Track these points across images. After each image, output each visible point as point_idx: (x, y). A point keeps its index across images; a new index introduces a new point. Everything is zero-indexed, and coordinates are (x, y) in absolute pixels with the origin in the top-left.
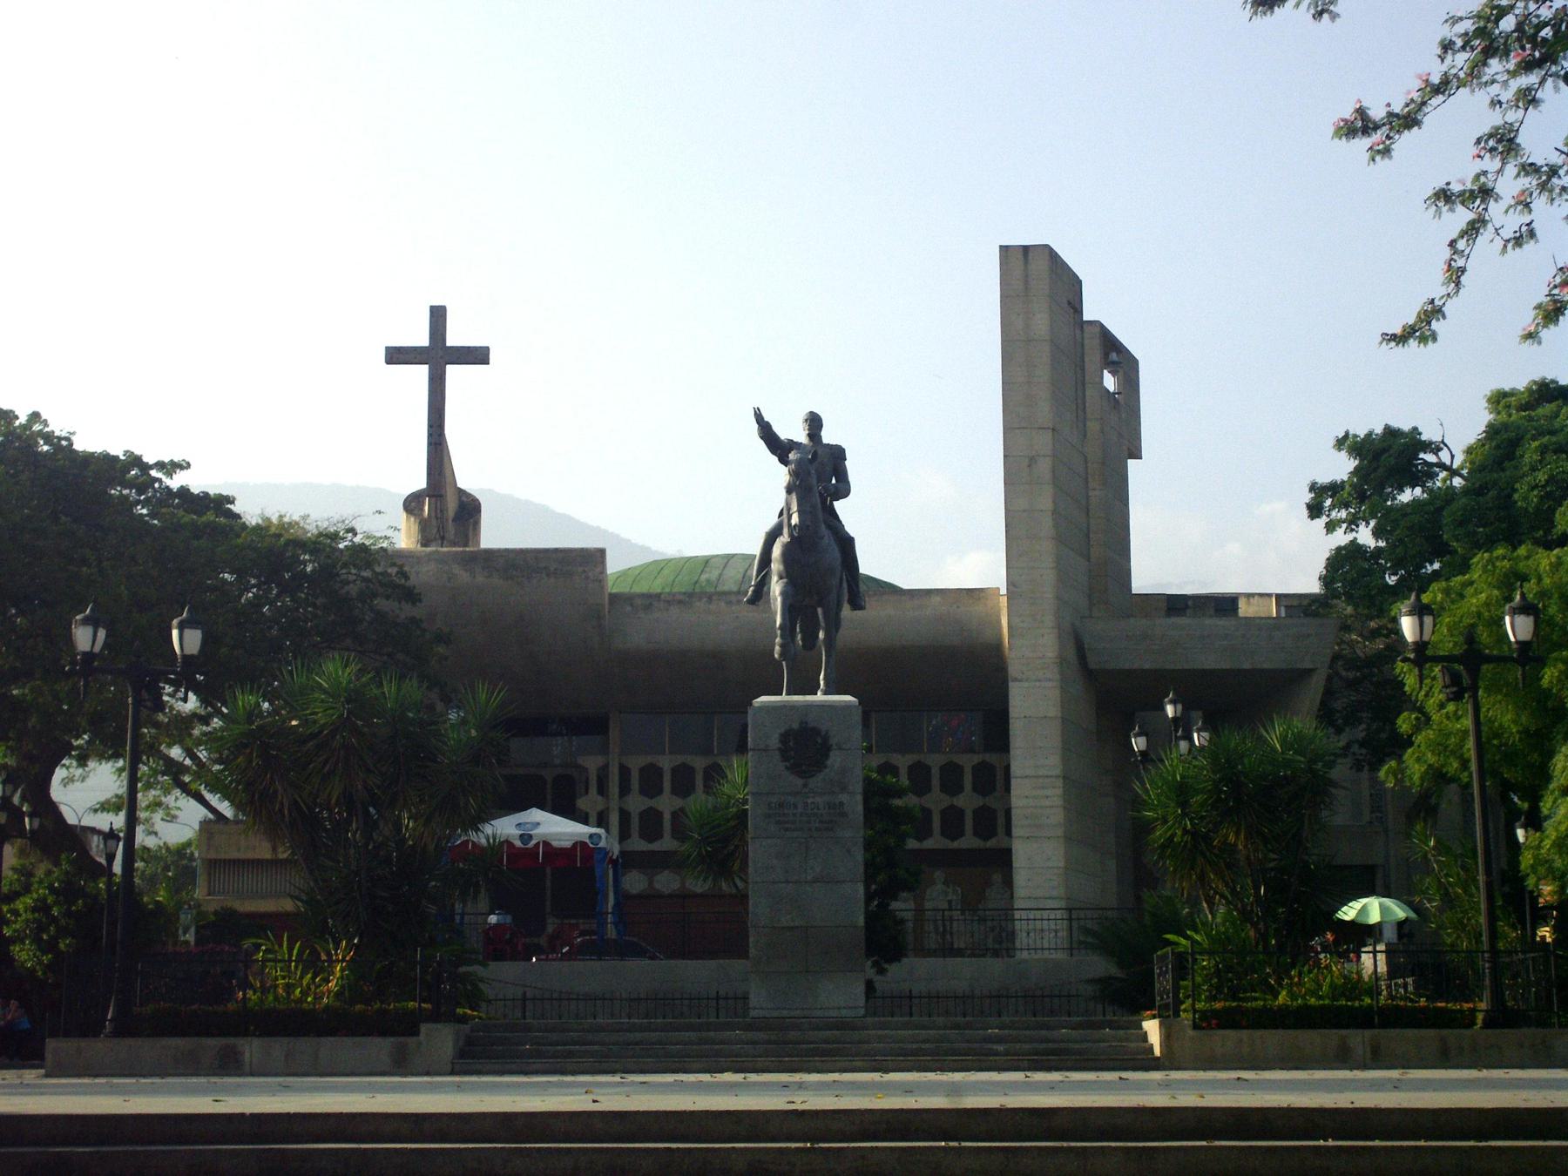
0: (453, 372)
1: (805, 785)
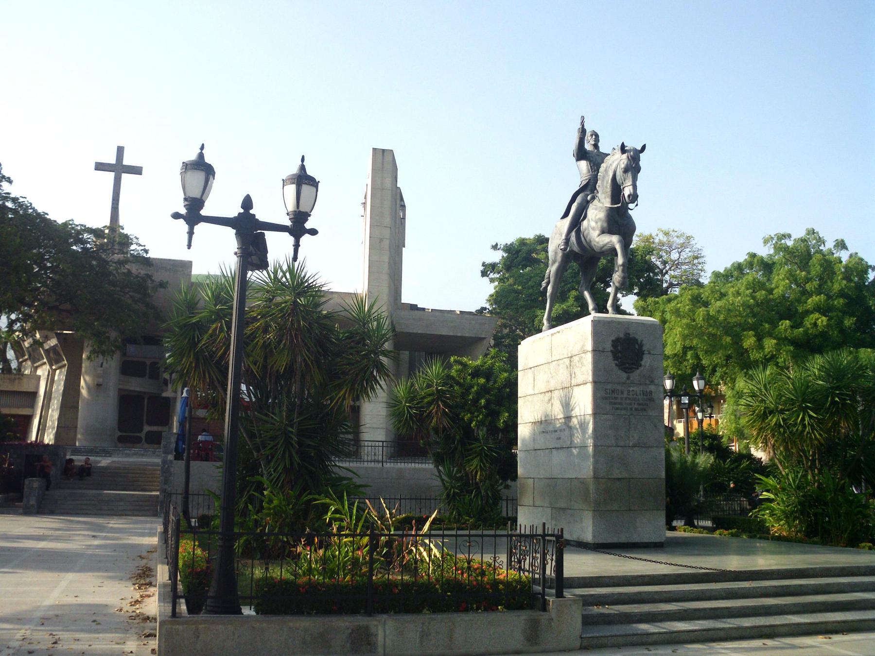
0: (125, 177)
1: (628, 378)
